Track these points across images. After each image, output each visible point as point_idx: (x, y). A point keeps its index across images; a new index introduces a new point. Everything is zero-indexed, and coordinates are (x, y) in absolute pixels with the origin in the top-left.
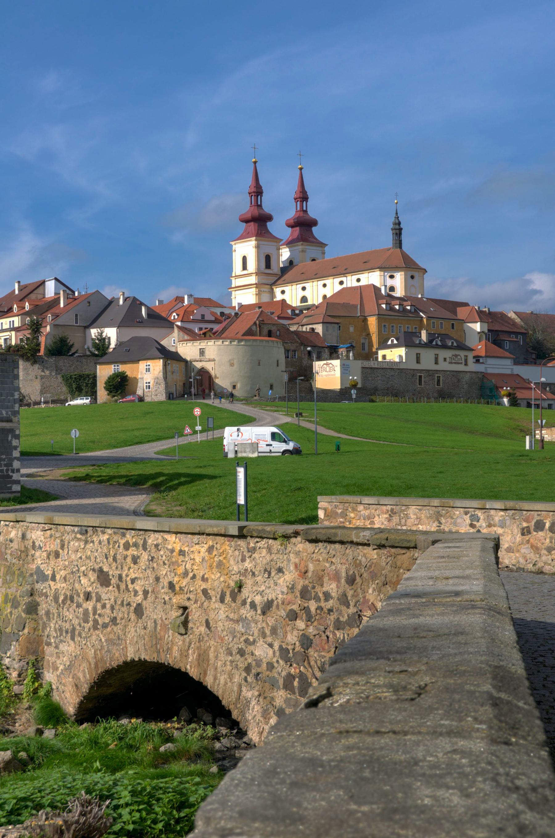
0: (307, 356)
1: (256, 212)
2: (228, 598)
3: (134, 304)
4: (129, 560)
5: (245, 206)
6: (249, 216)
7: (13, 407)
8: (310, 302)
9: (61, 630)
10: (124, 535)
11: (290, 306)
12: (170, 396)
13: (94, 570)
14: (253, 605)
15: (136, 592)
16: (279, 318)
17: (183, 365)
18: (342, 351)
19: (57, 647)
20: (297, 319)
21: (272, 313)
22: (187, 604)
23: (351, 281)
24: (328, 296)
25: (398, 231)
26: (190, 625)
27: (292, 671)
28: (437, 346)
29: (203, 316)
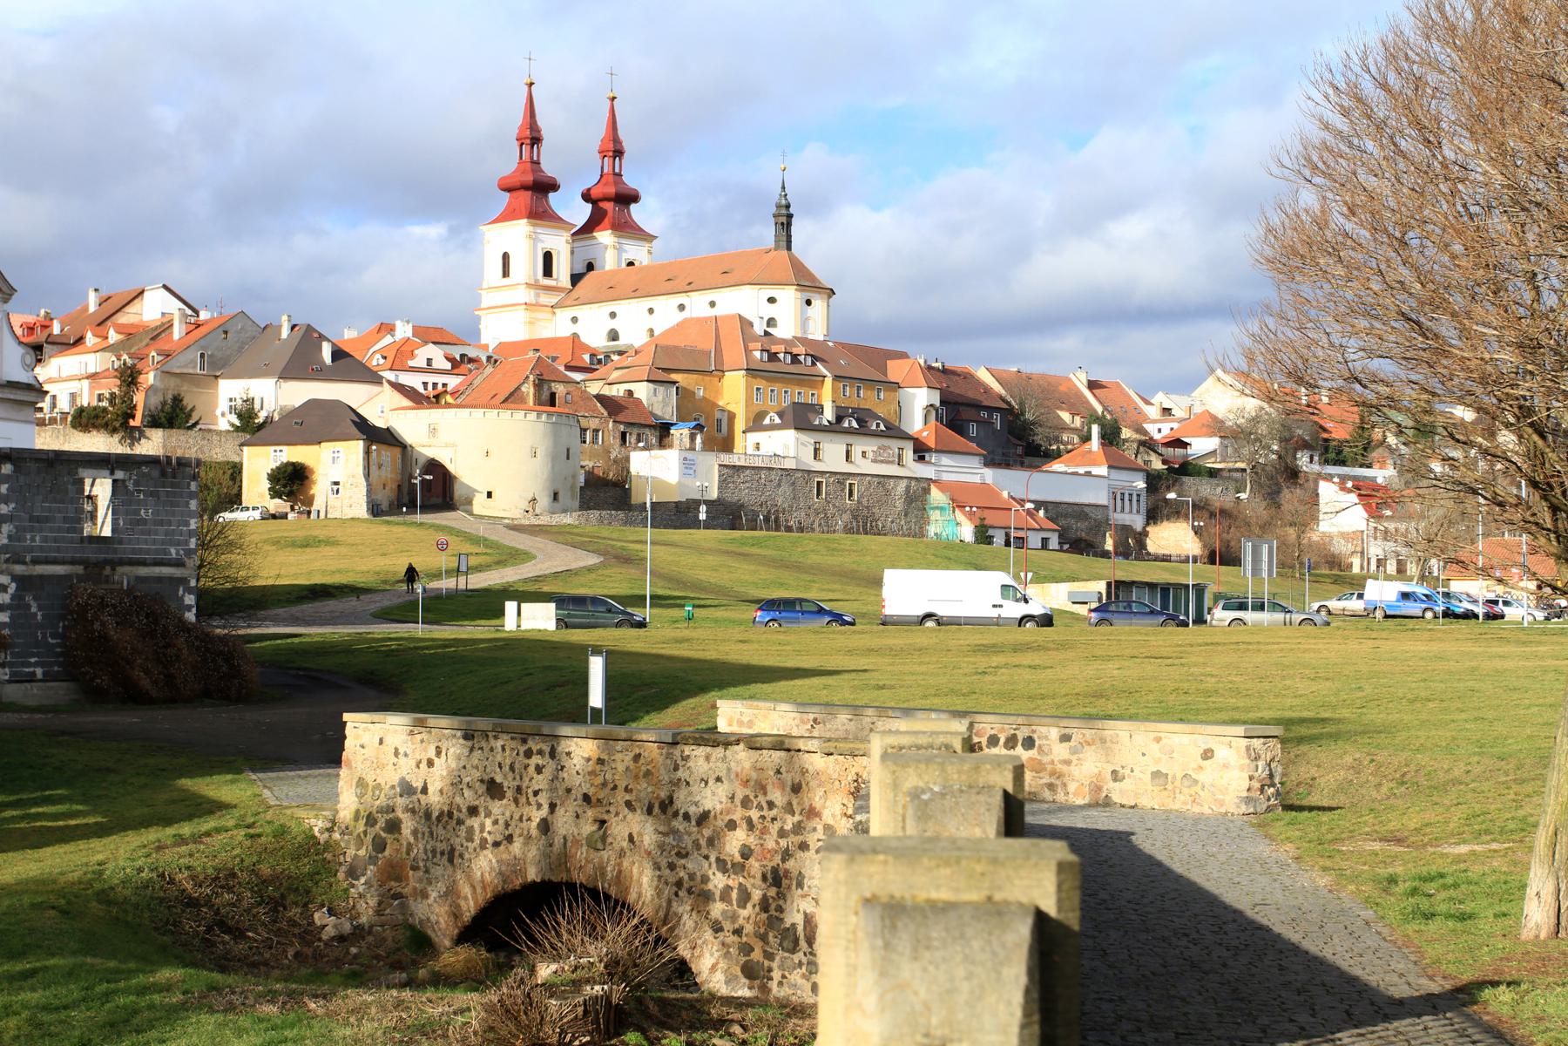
0: (618, 441)
1: (529, 178)
2: (656, 810)
3: (309, 338)
4: (532, 769)
5: (508, 162)
6: (516, 181)
7: (187, 543)
8: (623, 341)
9: (434, 851)
10: (524, 741)
11: (585, 348)
12: (375, 510)
13: (482, 781)
14: (687, 817)
15: (539, 806)
16: (568, 368)
17: (397, 451)
18: (680, 433)
19: (427, 871)
20: (602, 370)
21: (554, 359)
22: (606, 817)
23: (698, 305)
24: (656, 333)
25: (784, 220)
26: (609, 840)
27: (730, 883)
28: (850, 432)
29: (429, 361)
